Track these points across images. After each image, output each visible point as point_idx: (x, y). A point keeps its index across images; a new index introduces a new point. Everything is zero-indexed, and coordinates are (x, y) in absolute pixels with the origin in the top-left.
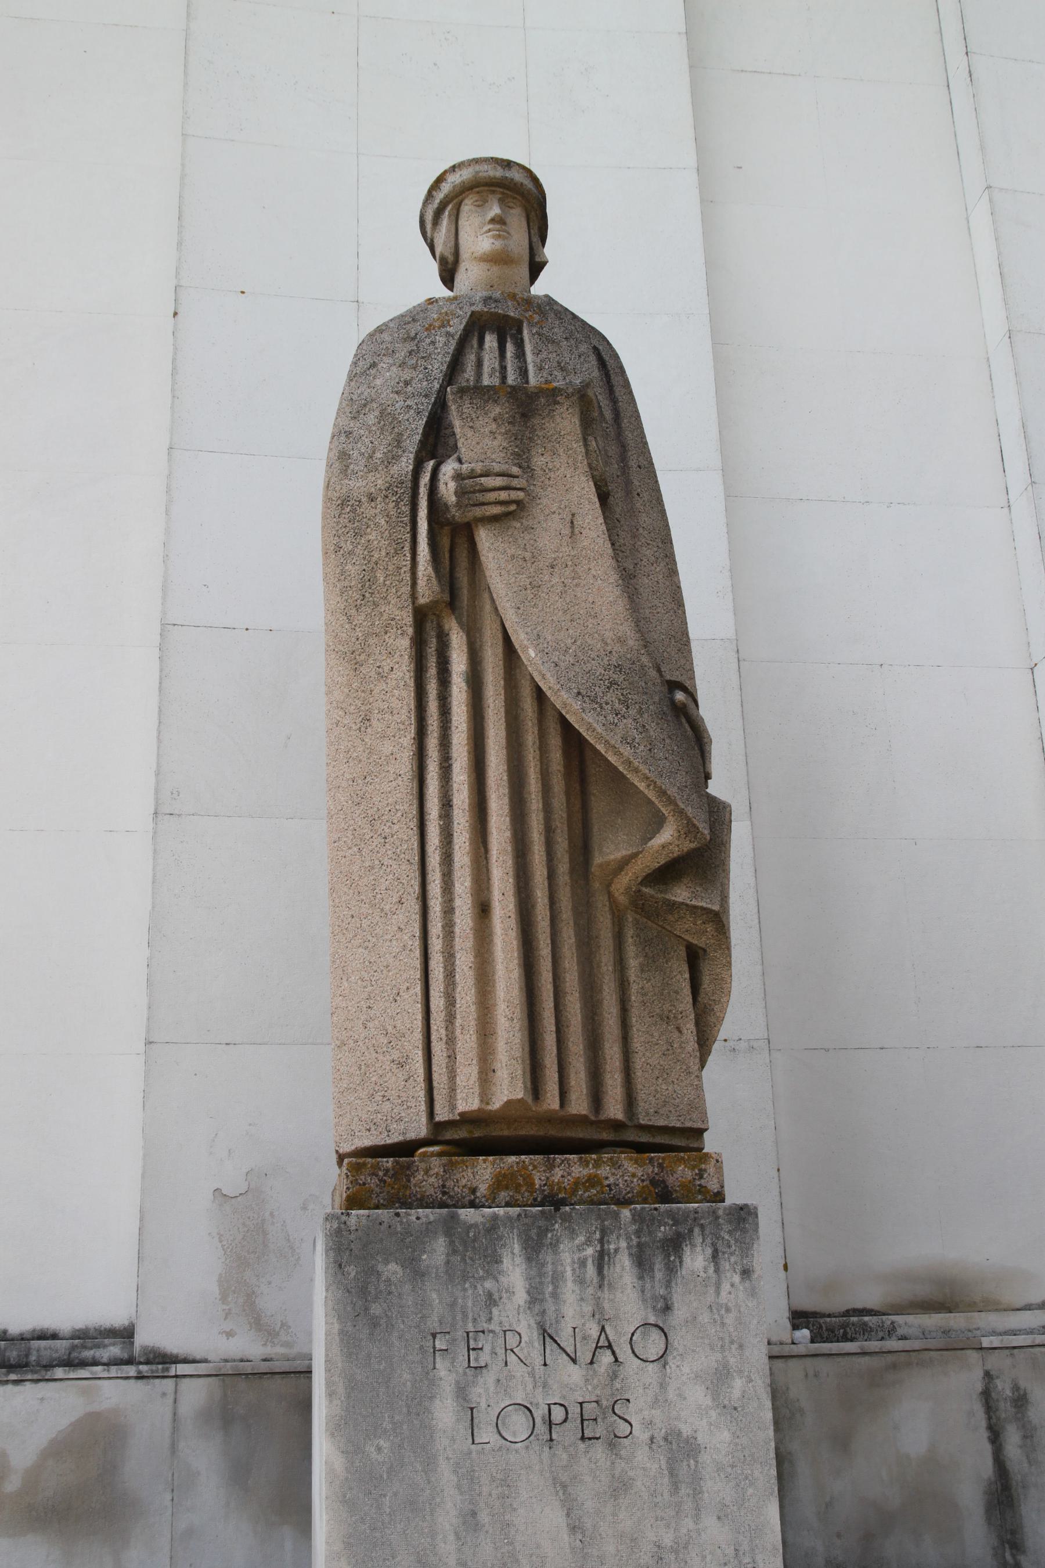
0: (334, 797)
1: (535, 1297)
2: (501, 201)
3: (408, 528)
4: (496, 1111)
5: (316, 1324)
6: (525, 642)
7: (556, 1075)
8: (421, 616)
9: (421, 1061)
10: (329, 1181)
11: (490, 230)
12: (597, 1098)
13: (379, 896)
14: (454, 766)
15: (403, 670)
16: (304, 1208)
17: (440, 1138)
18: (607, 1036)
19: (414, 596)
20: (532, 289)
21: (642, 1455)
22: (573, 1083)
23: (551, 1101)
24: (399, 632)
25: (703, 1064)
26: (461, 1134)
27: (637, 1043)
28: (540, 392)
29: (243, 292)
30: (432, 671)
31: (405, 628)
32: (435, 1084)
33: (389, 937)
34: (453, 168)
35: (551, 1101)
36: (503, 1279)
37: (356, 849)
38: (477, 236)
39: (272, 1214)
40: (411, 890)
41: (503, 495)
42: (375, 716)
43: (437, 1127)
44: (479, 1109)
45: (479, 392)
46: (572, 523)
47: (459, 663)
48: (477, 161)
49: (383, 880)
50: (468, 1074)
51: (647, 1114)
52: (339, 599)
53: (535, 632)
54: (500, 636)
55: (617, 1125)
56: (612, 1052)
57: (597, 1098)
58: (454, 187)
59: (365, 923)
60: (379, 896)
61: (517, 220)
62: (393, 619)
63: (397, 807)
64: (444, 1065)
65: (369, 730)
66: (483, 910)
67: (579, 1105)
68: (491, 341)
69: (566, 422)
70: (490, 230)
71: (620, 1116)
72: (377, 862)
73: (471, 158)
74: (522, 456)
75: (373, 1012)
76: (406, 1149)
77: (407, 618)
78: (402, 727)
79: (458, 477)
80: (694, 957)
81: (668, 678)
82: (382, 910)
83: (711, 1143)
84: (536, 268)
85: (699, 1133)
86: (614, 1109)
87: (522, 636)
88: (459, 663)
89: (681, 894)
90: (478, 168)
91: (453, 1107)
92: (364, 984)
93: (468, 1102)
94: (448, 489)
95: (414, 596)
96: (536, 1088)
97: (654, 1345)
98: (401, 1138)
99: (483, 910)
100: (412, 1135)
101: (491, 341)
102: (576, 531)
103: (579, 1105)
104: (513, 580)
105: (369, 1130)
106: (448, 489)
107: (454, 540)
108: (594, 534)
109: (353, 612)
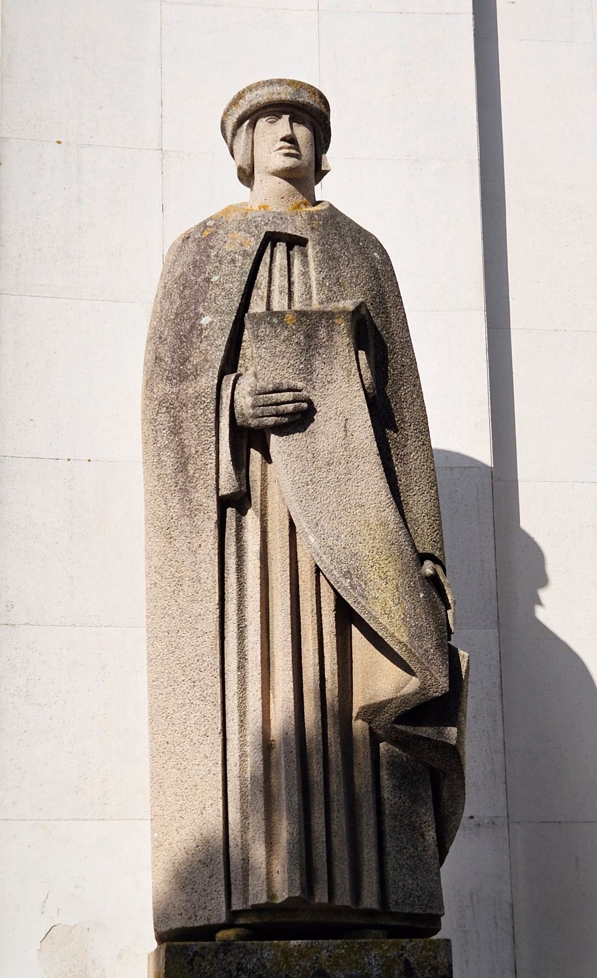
0: (152, 644)
2: (291, 121)
3: (213, 433)
4: (281, 903)
6: (306, 530)
7: (326, 876)
9: (222, 863)
11: (281, 148)
13: (189, 728)
14: (249, 628)
16: (120, 957)
17: (236, 923)
18: (365, 843)
19: (218, 489)
20: (317, 188)
22: (338, 881)
24: (206, 516)
25: (442, 862)
27: (390, 845)
28: (322, 314)
29: (59, 142)
31: (211, 514)
32: (232, 881)
33: (196, 762)
34: (250, 89)
35: (321, 896)
37: (170, 689)
38: (271, 139)
39: (93, 962)
40: (214, 726)
41: (290, 407)
42: (186, 582)
43: (233, 915)
44: (266, 903)
46: (345, 427)
48: (271, 83)
49: (192, 716)
51: (397, 904)
52: (156, 483)
53: (315, 521)
54: (287, 522)
55: (370, 913)
56: (369, 854)
58: (251, 106)
59: (178, 749)
60: (189, 728)
61: (302, 133)
62: (201, 505)
63: (204, 658)
64: (240, 866)
65: (181, 594)
67: (344, 899)
69: (343, 340)
70: (281, 148)
71: (375, 906)
72: (187, 701)
73: (265, 79)
74: (308, 372)
75: (184, 821)
78: (209, 594)
81: (421, 551)
82: (192, 740)
83: (447, 929)
85: (433, 922)
87: (304, 524)
90: (271, 89)
91: (246, 900)
92: (178, 798)
95: (218, 489)
98: (206, 922)
100: (214, 921)
101: (281, 249)
102: (349, 434)
103: (344, 899)
104: (297, 478)
105: (181, 914)
108: (363, 436)
109: (169, 496)
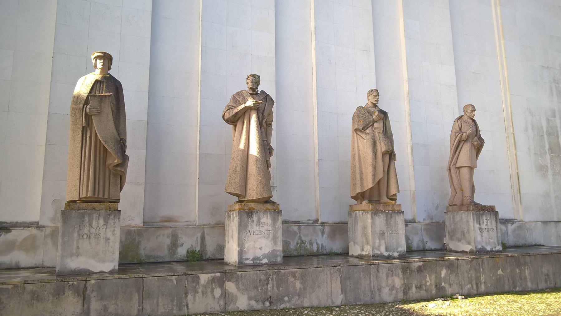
1: (89, 221)
5: (60, 225)
8: (83, 128)
10: (354, 110)
12: (104, 195)
15: (80, 135)
21: (102, 240)
23: (96, 196)
26: (84, 199)
27: (111, 188)
30: (84, 135)
35: (96, 196)
36: (402, 282)
45: (95, 96)
47: (88, 135)
50: (84, 192)
56: (107, 189)
57: (104, 195)
66: (89, 170)
67: (101, 196)
68: (98, 84)
76: (75, 201)
77: (81, 128)
79: (89, 109)
80: (121, 177)
84: (109, 69)
86: (106, 197)
88: (88, 135)
89: (118, 169)
93: (84, 195)
94: (88, 110)
96: (94, 194)
97: (105, 227)
99: (89, 170)
101: (98, 84)
106: (88, 110)
107: (88, 118)
